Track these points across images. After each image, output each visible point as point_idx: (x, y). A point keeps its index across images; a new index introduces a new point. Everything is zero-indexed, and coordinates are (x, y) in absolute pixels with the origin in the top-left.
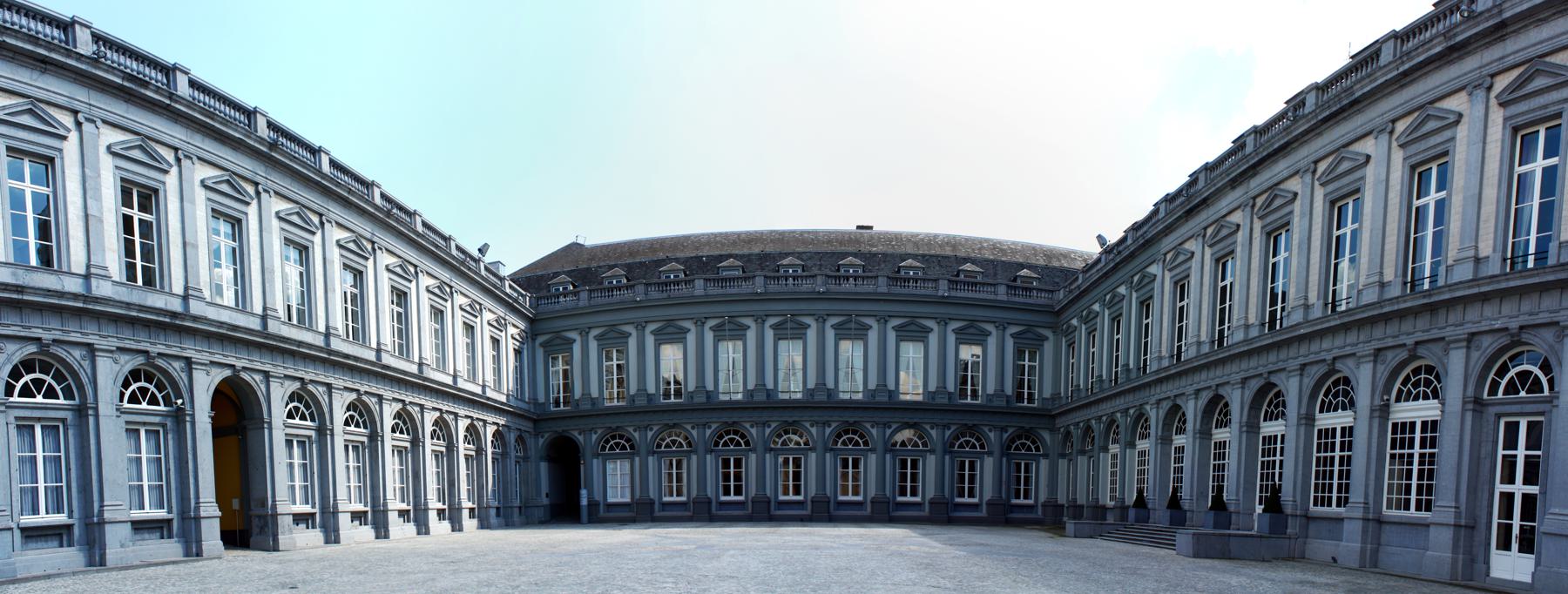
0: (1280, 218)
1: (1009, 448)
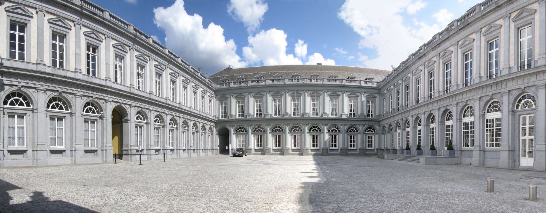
0: (448, 59)
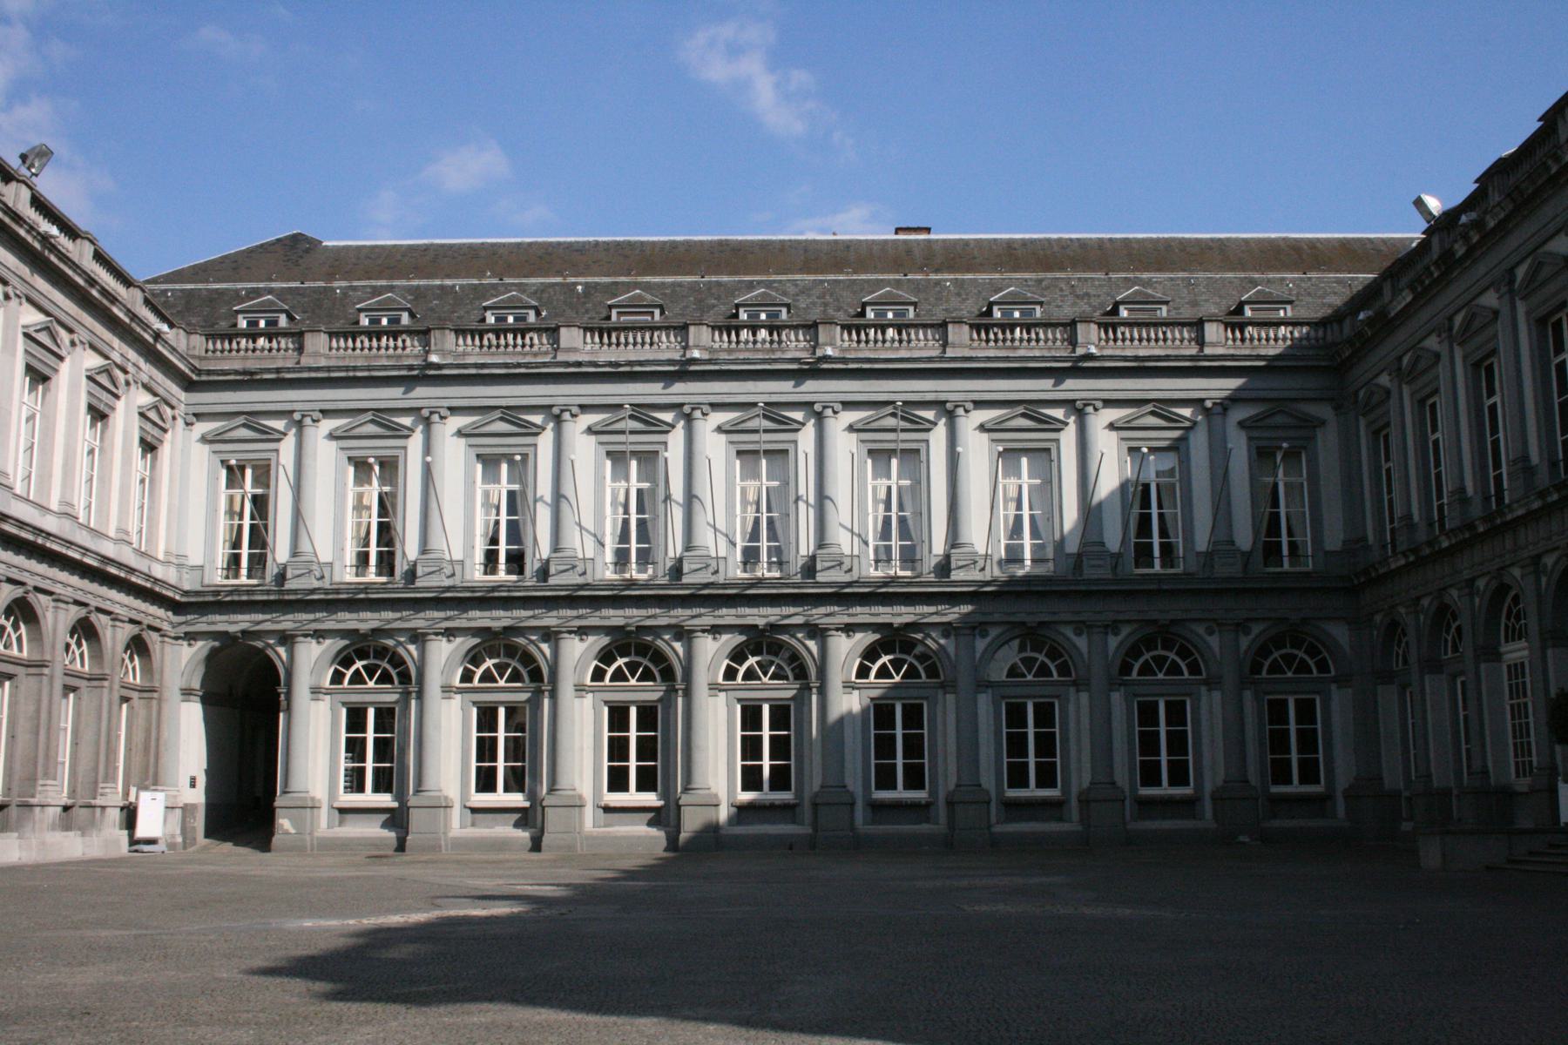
1: (1257, 667)
